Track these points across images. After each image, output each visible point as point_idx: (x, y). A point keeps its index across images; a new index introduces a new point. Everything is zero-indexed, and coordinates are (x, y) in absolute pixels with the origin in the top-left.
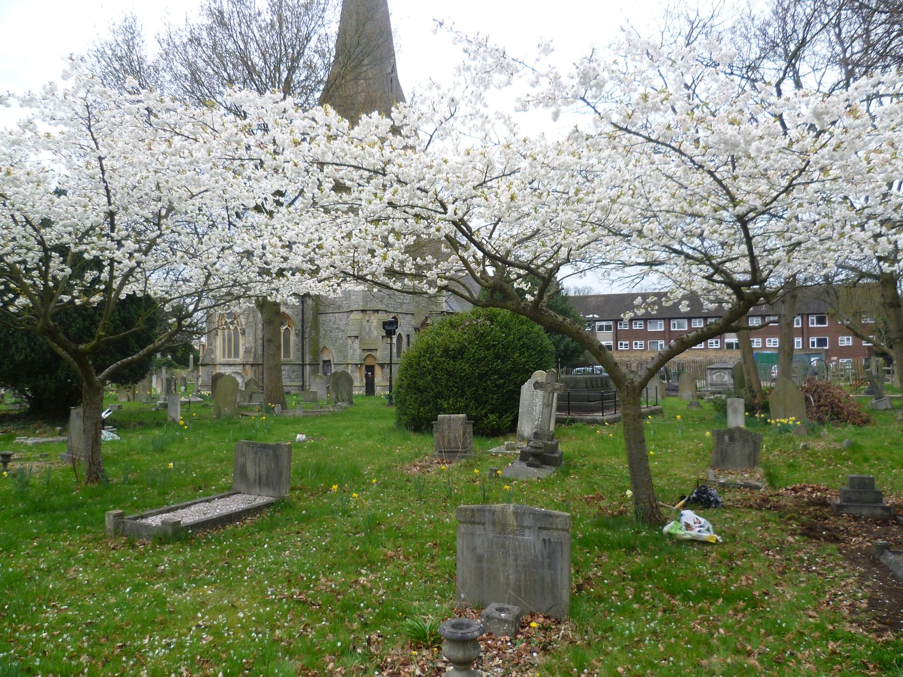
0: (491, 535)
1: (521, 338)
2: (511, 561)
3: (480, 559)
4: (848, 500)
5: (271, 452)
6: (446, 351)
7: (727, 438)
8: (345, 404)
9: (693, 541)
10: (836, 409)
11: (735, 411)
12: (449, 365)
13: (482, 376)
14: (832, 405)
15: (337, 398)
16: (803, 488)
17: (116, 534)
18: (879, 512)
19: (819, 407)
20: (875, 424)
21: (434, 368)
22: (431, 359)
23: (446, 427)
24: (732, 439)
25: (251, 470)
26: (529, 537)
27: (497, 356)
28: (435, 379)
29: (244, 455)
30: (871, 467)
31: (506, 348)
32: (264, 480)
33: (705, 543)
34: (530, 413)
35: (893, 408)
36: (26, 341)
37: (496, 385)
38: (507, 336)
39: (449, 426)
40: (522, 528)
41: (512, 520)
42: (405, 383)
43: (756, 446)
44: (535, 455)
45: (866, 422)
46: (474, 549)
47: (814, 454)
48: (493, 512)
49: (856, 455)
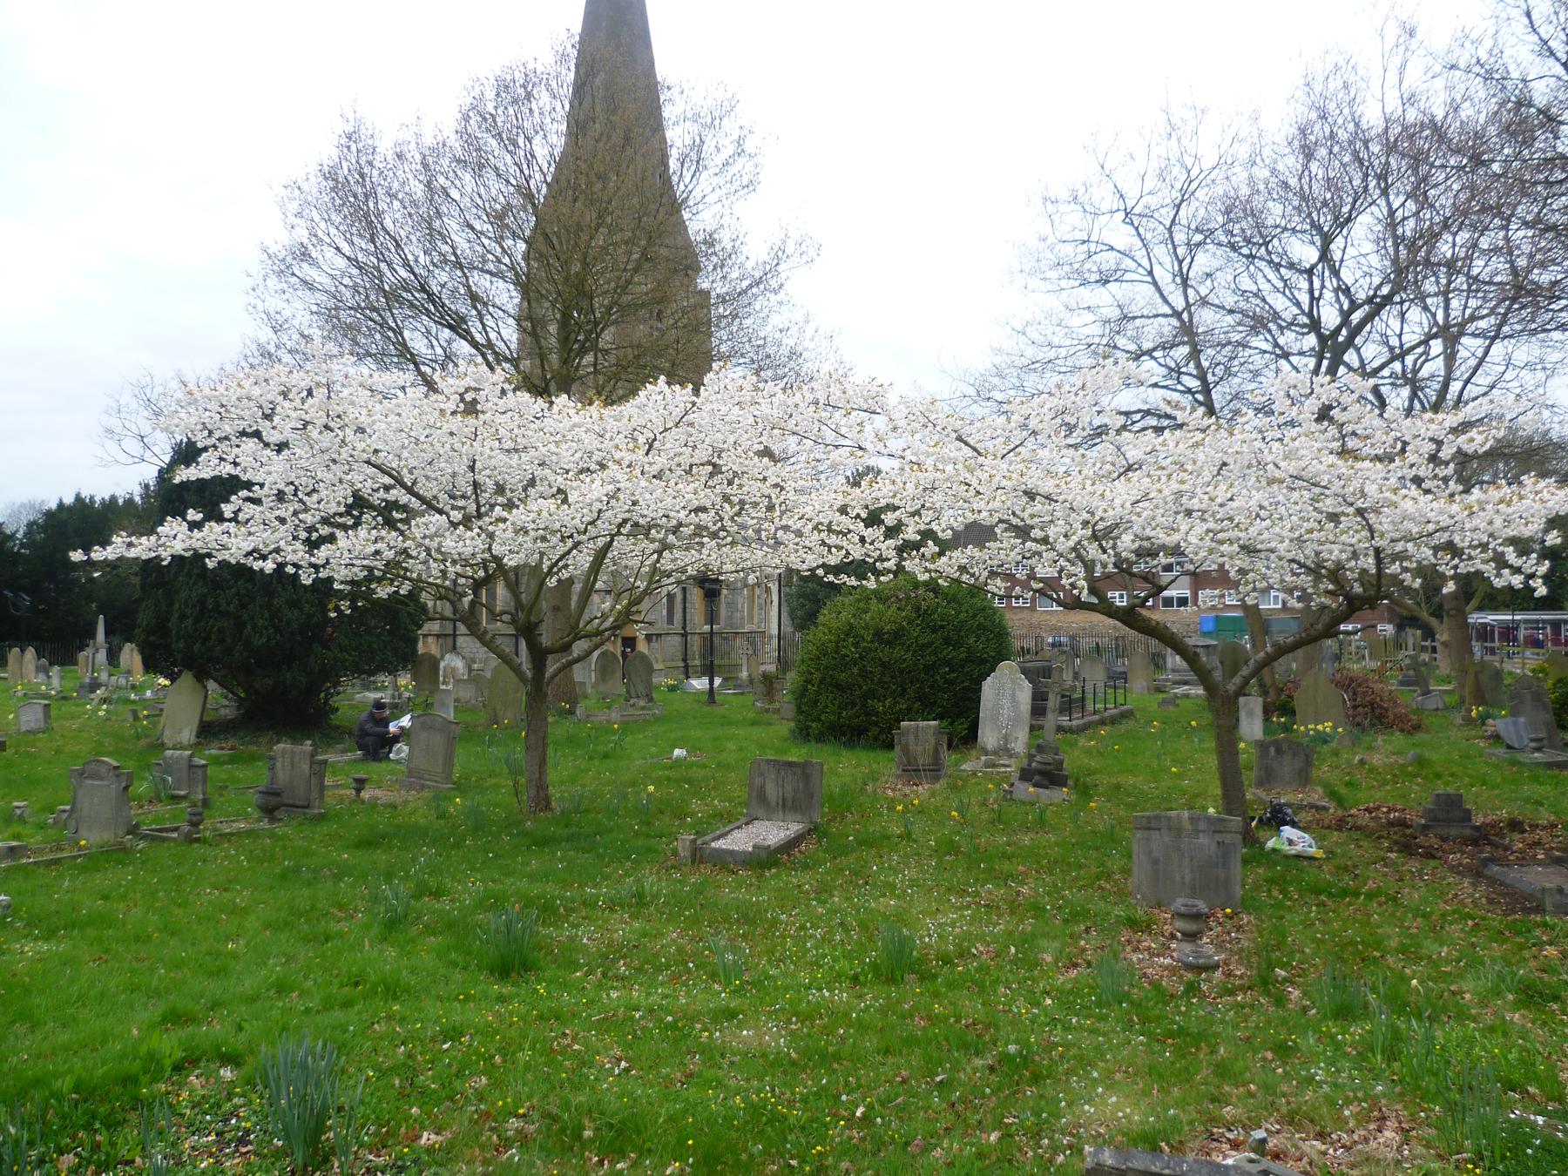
0: (1167, 839)
1: (975, 616)
2: (1186, 862)
3: (1155, 862)
4: (1435, 820)
5: (799, 771)
6: (878, 634)
7: (1272, 750)
8: (642, 703)
9: (1298, 856)
10: (1378, 711)
11: (1251, 714)
12: (885, 653)
13: (929, 669)
14: (1372, 705)
15: (628, 692)
16: (1377, 808)
17: (693, 862)
18: (1468, 832)
19: (1355, 707)
20: (1428, 732)
21: (861, 657)
22: (856, 645)
23: (911, 737)
24: (1279, 751)
25: (771, 791)
26: (1203, 840)
27: (947, 641)
28: (864, 673)
29: (762, 774)
30: (1447, 784)
31: (958, 630)
32: (789, 803)
33: (1311, 858)
34: (995, 718)
35: (1446, 708)
36: (267, 615)
37: (947, 681)
38: (958, 614)
39: (916, 737)
40: (1197, 832)
41: (1187, 825)
42: (817, 676)
43: (1308, 763)
44: (1042, 773)
45: (1417, 728)
46: (1150, 853)
47: (1372, 770)
48: (1169, 818)
49: (1424, 772)
